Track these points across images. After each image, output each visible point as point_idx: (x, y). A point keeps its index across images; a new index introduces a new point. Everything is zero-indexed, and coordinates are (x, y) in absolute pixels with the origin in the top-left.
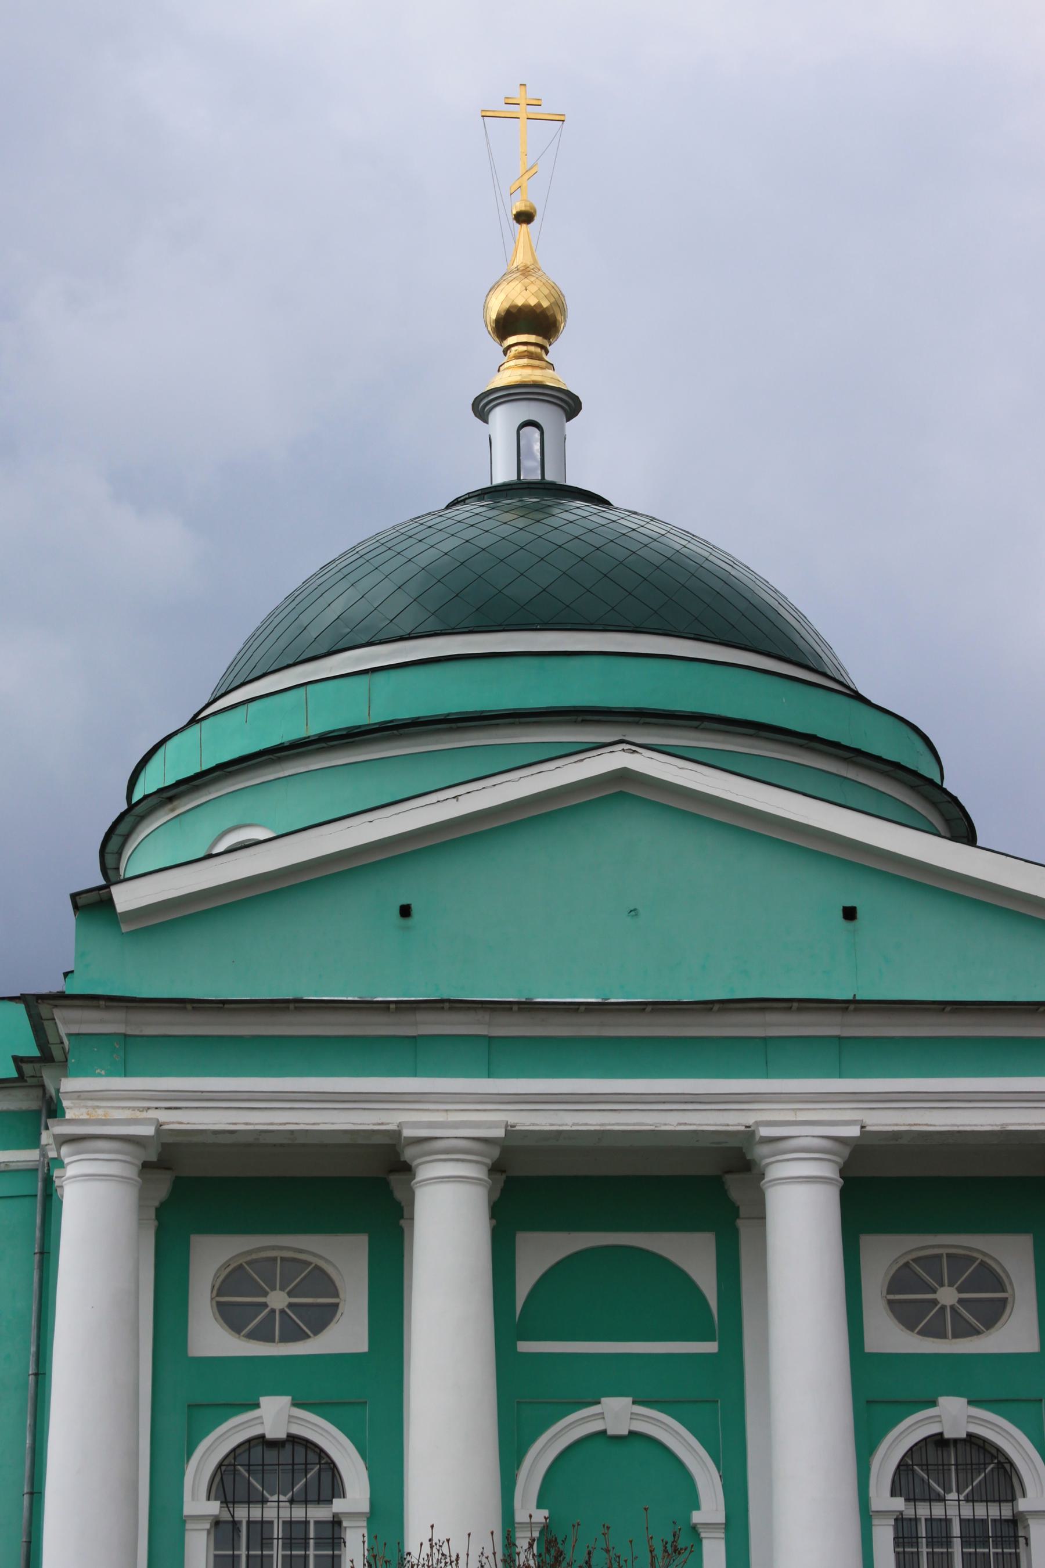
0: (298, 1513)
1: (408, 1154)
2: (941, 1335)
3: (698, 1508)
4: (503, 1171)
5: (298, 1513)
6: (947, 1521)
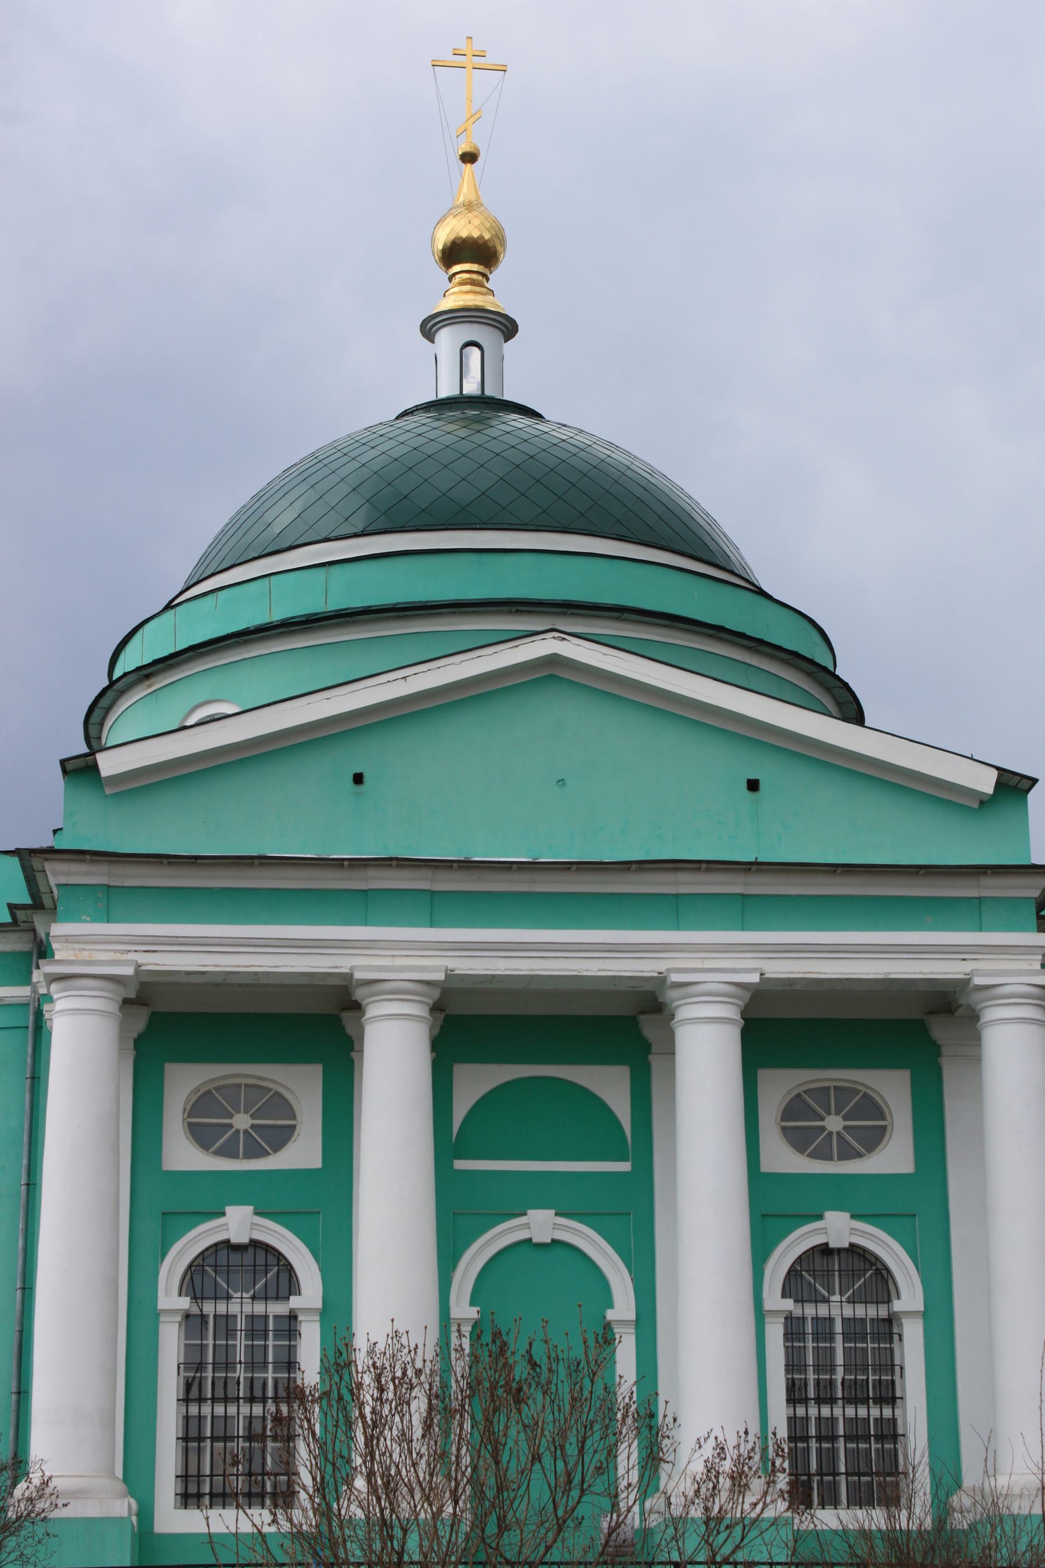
0: (259, 1308)
1: (359, 994)
2: (828, 1157)
5: (259, 1308)
6: (831, 1320)
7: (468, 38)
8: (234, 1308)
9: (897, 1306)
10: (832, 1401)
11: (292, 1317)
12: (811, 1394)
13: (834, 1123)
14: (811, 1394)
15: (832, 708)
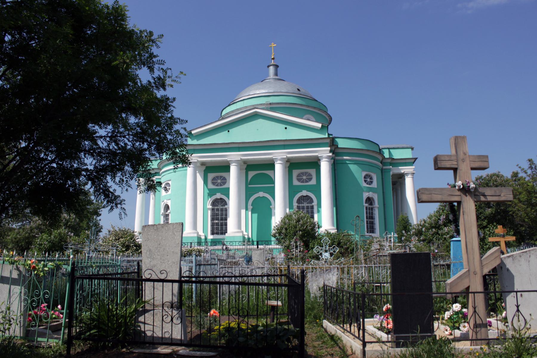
0: (308, 205)
1: (320, 158)
2: (304, 182)
3: (271, 205)
4: (205, 165)
5: (308, 205)
6: (219, 209)
7: (181, 72)
8: (304, 205)
9: (375, 206)
10: (222, 220)
11: (313, 206)
12: (220, 219)
13: (304, 177)
14: (220, 219)
15: (314, 120)
